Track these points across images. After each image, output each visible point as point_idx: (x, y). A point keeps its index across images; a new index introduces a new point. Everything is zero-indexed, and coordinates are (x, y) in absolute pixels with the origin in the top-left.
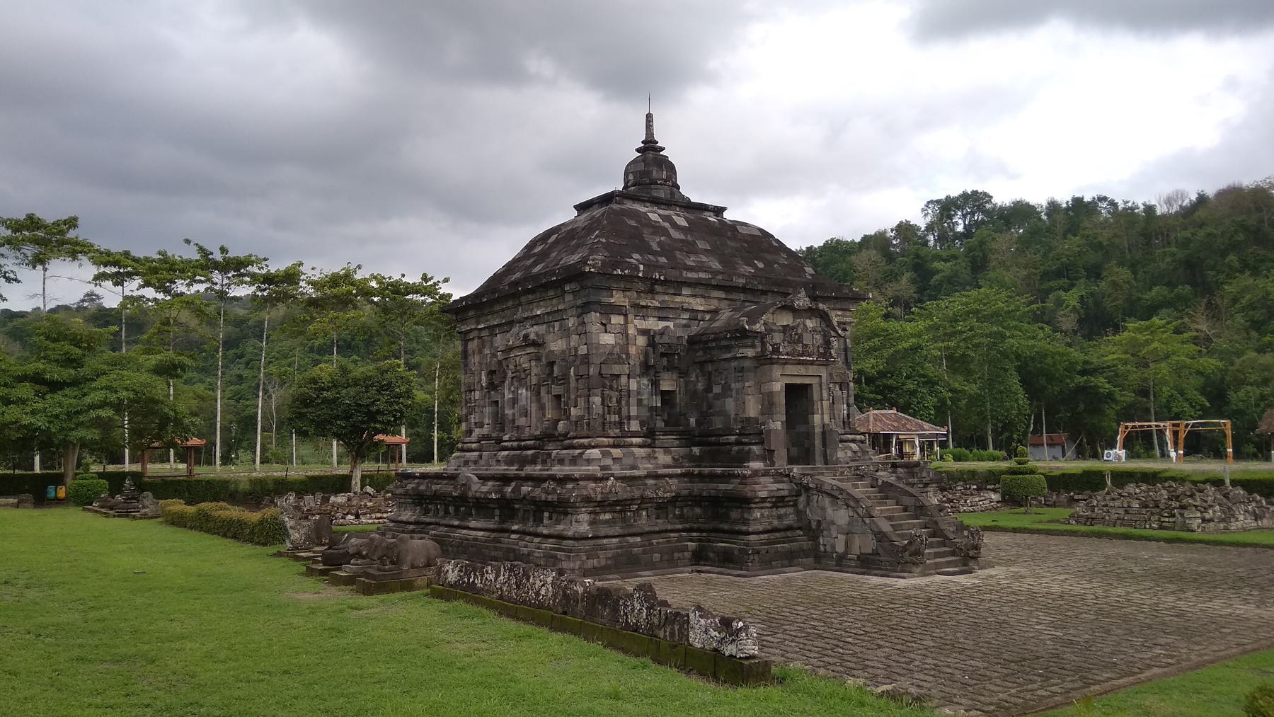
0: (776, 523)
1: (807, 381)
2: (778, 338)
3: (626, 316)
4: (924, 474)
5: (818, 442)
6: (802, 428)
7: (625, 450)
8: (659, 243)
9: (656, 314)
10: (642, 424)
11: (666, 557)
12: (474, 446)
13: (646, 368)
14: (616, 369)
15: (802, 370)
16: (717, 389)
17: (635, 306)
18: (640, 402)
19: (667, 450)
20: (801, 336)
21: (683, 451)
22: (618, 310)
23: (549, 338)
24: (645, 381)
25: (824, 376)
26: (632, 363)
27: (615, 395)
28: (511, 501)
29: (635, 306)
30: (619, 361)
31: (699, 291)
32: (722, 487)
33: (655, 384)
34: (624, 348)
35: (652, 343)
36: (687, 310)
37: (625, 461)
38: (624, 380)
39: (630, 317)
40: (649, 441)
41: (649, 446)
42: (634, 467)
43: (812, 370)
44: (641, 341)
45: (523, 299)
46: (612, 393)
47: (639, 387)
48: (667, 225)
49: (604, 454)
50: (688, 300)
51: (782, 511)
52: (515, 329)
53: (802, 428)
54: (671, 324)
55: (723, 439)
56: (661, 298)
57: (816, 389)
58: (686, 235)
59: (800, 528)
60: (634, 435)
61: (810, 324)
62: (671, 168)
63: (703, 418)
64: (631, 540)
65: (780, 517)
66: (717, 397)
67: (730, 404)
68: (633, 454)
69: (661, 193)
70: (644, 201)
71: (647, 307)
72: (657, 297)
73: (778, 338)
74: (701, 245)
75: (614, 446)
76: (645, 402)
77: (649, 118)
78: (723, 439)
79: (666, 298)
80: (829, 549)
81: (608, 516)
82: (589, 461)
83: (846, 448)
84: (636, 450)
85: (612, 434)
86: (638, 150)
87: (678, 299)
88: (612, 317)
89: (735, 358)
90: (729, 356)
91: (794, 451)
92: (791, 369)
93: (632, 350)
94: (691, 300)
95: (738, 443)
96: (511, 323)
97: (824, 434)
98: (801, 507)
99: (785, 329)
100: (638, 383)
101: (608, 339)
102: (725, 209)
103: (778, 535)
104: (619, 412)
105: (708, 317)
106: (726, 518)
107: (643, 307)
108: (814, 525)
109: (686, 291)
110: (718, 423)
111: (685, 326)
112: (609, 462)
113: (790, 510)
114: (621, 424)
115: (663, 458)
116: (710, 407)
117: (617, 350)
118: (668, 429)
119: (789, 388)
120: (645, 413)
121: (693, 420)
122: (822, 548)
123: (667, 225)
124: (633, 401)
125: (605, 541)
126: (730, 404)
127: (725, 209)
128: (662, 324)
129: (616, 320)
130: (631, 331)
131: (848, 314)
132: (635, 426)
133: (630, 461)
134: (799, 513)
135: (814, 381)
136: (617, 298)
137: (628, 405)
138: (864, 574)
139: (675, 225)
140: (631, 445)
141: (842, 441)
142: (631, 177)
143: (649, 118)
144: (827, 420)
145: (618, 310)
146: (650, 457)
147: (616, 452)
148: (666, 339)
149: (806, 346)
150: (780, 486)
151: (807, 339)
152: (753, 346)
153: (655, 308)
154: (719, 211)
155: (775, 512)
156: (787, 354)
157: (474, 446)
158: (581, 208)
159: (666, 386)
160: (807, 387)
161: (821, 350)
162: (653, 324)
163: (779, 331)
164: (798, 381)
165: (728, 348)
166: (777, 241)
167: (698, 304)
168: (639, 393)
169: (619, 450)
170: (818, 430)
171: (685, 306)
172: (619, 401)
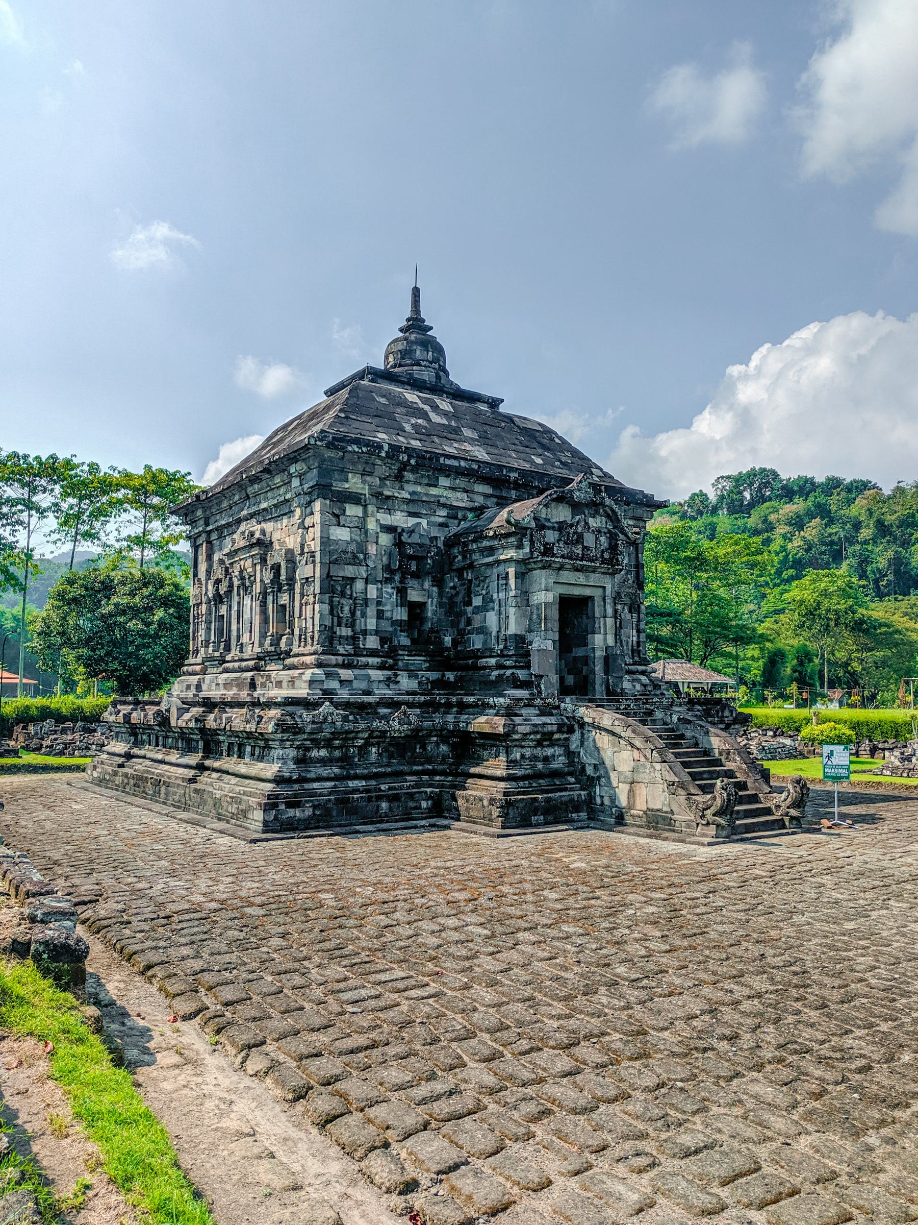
0: (540, 766)
1: (587, 592)
2: (551, 536)
3: (365, 506)
4: (727, 713)
5: (599, 668)
6: (579, 652)
7: (357, 672)
8: (414, 426)
10: (383, 641)
12: (198, 668)
15: (581, 578)
16: (477, 601)
17: (377, 495)
18: (380, 615)
19: (412, 675)
20: (580, 537)
21: (433, 676)
22: (355, 499)
24: (388, 589)
25: (609, 587)
26: (371, 564)
28: (215, 732)
29: (377, 495)
30: (355, 561)
31: (460, 482)
33: (402, 592)
34: (362, 547)
35: (399, 544)
36: (444, 506)
37: (356, 684)
38: (359, 585)
39: (371, 508)
40: (391, 661)
41: (390, 668)
42: (368, 693)
43: (594, 579)
44: (385, 539)
45: (250, 490)
46: (344, 601)
47: (380, 595)
48: (427, 408)
49: (328, 675)
51: (549, 752)
52: (242, 527)
53: (579, 652)
54: (424, 522)
55: (483, 662)
56: (411, 488)
57: (598, 601)
58: (448, 419)
59: (571, 774)
60: (373, 653)
61: (594, 523)
62: (439, 350)
63: (461, 638)
64: (352, 784)
65: (546, 759)
66: (477, 610)
67: (492, 619)
68: (368, 677)
69: (427, 375)
70: (403, 383)
72: (406, 486)
73: (551, 536)
74: (467, 433)
75: (344, 666)
76: (388, 614)
77: (416, 292)
78: (483, 662)
79: (419, 489)
80: (607, 802)
83: (634, 680)
85: (342, 651)
86: (401, 330)
87: (434, 491)
88: (347, 506)
89: (498, 562)
90: (491, 559)
91: (570, 680)
92: (567, 576)
93: (372, 549)
96: (239, 522)
97: (606, 659)
98: (573, 747)
99: (561, 527)
100: (380, 590)
102: (502, 401)
104: (352, 625)
105: (470, 516)
107: (388, 497)
108: (590, 771)
109: (444, 481)
110: (477, 642)
111: (441, 525)
112: (334, 684)
113: (558, 751)
114: (354, 639)
115: (406, 683)
116: (469, 622)
117: (353, 548)
121: (448, 640)
122: (598, 801)
123: (427, 408)
124: (371, 611)
125: (316, 785)
126: (492, 619)
127: (502, 401)
128: (412, 521)
129: (353, 511)
130: (372, 525)
132: (372, 642)
133: (363, 685)
134: (570, 754)
135: (597, 593)
137: (364, 615)
138: (650, 836)
139: (435, 408)
140: (366, 666)
141: (629, 672)
142: (391, 359)
143: (416, 292)
144: (611, 641)
145: (355, 499)
146: (388, 681)
147: (345, 674)
148: (415, 539)
149: (588, 548)
150: (546, 719)
151: (589, 540)
154: (494, 403)
155: (538, 752)
156: (563, 557)
157: (198, 668)
158: (331, 392)
159: (414, 596)
160: (585, 601)
161: (606, 555)
162: (400, 519)
163: (553, 528)
164: (577, 591)
166: (560, 438)
167: (459, 500)
168: (379, 603)
169: (350, 672)
170: (599, 654)
171: (442, 500)
172: (353, 613)
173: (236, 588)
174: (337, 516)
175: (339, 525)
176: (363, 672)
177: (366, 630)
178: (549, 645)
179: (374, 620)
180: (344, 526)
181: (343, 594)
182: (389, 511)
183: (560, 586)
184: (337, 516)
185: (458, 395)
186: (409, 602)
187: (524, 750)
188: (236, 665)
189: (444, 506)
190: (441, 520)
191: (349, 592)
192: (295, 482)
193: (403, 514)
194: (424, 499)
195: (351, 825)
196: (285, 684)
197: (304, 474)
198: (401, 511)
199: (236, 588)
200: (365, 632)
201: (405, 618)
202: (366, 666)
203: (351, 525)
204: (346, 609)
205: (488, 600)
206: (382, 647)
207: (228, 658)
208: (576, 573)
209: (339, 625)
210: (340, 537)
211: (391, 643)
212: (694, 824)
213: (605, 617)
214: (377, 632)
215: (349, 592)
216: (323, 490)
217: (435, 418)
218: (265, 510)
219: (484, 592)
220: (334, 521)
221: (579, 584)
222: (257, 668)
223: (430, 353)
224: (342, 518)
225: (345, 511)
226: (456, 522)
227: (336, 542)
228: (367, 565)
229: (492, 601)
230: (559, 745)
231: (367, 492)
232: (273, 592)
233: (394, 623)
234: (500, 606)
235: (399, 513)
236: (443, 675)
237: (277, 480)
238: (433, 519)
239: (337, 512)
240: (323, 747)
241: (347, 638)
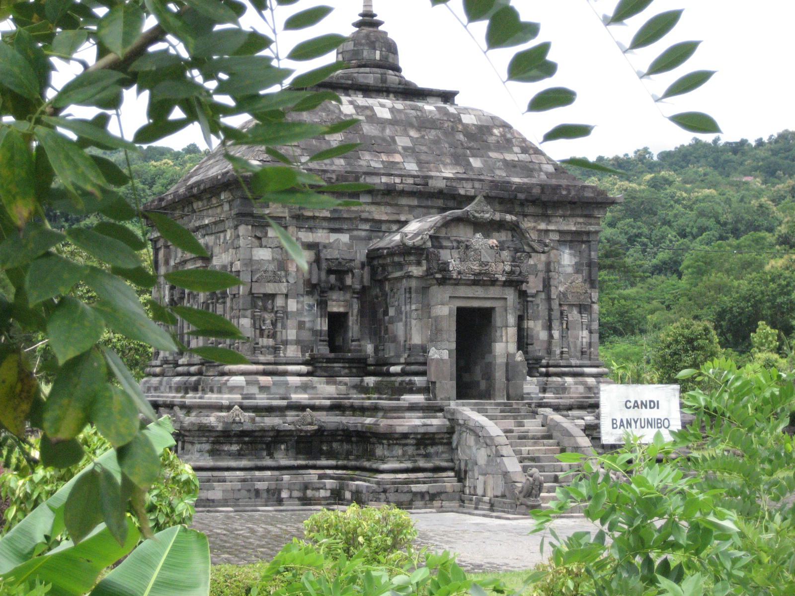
1: (488, 304)
7: (276, 378)
9: (325, 224)
11: (296, 494)
12: (158, 370)
13: (312, 288)
14: (270, 288)
15: (479, 291)
18: (301, 325)
23: (216, 250)
26: (292, 281)
27: (268, 317)
30: (276, 280)
32: (369, 421)
36: (366, 220)
37: (274, 390)
38: (279, 302)
50: (368, 208)
62: (391, 48)
68: (286, 383)
71: (314, 218)
75: (265, 373)
76: (308, 325)
81: (235, 448)
82: (232, 389)
84: (291, 379)
92: (463, 291)
94: (373, 208)
95: (404, 373)
101: (263, 254)
103: (420, 475)
104: (273, 336)
106: (371, 456)
107: (309, 218)
109: (365, 199)
118: (332, 355)
119: (461, 312)
120: (306, 335)
124: (291, 323)
125: (226, 474)
131: (593, 221)
133: (282, 391)
136: (275, 209)
140: (285, 373)
146: (304, 388)
152: (419, 264)
153: (325, 219)
154: (448, 97)
157: (158, 370)
162: (321, 236)
164: (476, 304)
165: (400, 266)
169: (269, 378)
171: (364, 215)
172: (274, 324)
173: (186, 295)
174: (259, 238)
175: (261, 246)
176: (282, 378)
177: (287, 340)
178: (445, 355)
179: (294, 332)
180: (266, 247)
181: (265, 309)
182: (310, 229)
183: (457, 300)
184: (259, 238)
185: (411, 93)
186: (329, 312)
187: (406, 448)
188: (186, 368)
189: (366, 220)
190: (363, 234)
191: (270, 307)
192: (226, 207)
193: (325, 231)
194: (345, 216)
195: (256, 506)
196: (215, 389)
197: (233, 200)
198: (323, 229)
199: (186, 295)
200: (286, 343)
201: (325, 328)
202: (285, 373)
203: (272, 246)
204: (268, 322)
205: (399, 311)
206: (303, 355)
207: (180, 362)
208: (474, 287)
209: (262, 336)
210: (262, 257)
211: (312, 351)
212: (514, 505)
213: (507, 326)
214: (298, 342)
215: (270, 307)
216: (244, 217)
217: (368, 129)
218: (207, 225)
219: (396, 303)
220: (256, 242)
221: (476, 298)
222: (200, 373)
223: (378, 53)
224: (264, 241)
225: (266, 233)
226: (381, 234)
227: (260, 262)
228: (288, 282)
229: (401, 313)
230: (442, 444)
231: (287, 215)
232: (212, 303)
233: (315, 333)
234: (406, 318)
235: (321, 231)
236: (362, 381)
237: (214, 201)
238: (355, 233)
239: (259, 234)
240: (234, 443)
241: (268, 347)
